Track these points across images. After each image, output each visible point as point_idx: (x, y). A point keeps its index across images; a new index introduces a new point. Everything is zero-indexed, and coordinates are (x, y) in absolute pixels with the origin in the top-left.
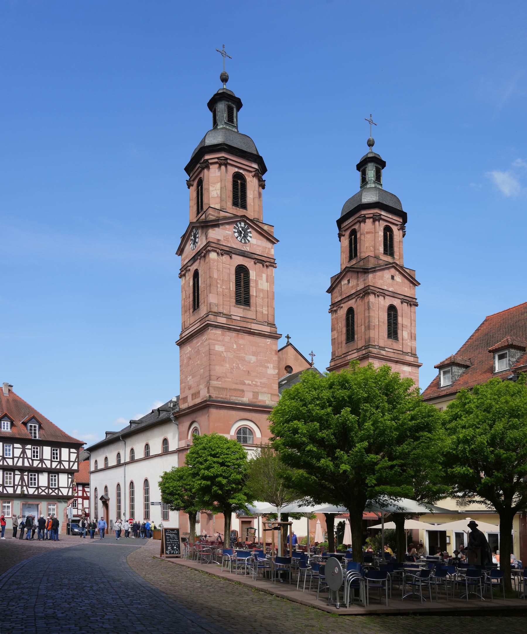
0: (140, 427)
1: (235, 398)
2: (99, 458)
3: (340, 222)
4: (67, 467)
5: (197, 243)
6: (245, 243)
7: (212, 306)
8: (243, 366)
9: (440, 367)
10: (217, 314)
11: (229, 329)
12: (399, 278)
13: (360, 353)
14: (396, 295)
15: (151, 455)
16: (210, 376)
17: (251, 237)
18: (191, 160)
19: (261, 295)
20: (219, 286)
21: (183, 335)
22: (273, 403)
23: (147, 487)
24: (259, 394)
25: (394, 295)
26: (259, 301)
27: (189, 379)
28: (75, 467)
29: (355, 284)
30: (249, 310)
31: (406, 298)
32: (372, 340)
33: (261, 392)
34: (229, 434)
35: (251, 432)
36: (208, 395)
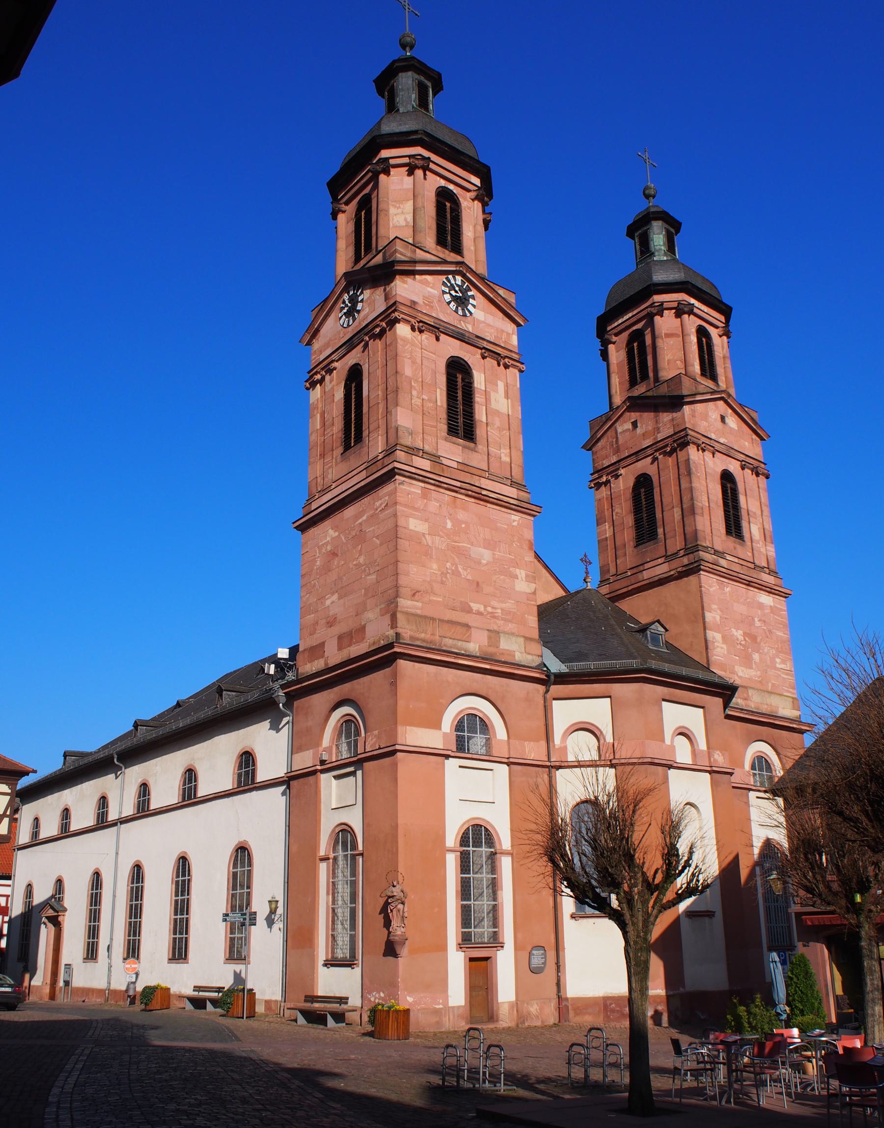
0: (86, 762)
1: (451, 641)
5: (358, 312)
6: (464, 315)
7: (400, 433)
8: (466, 570)
10: (412, 451)
11: (439, 485)
12: (732, 422)
13: (676, 564)
14: (732, 453)
15: (109, 819)
16: (397, 587)
17: (474, 306)
18: (341, 169)
19: (497, 423)
20: (414, 393)
21: (314, 506)
22: (530, 657)
24: (502, 635)
25: (728, 452)
26: (493, 433)
27: (328, 602)
29: (650, 428)
30: (474, 450)
31: (749, 460)
32: (700, 535)
33: (505, 633)
34: (440, 728)
35: (485, 726)
36: (391, 633)
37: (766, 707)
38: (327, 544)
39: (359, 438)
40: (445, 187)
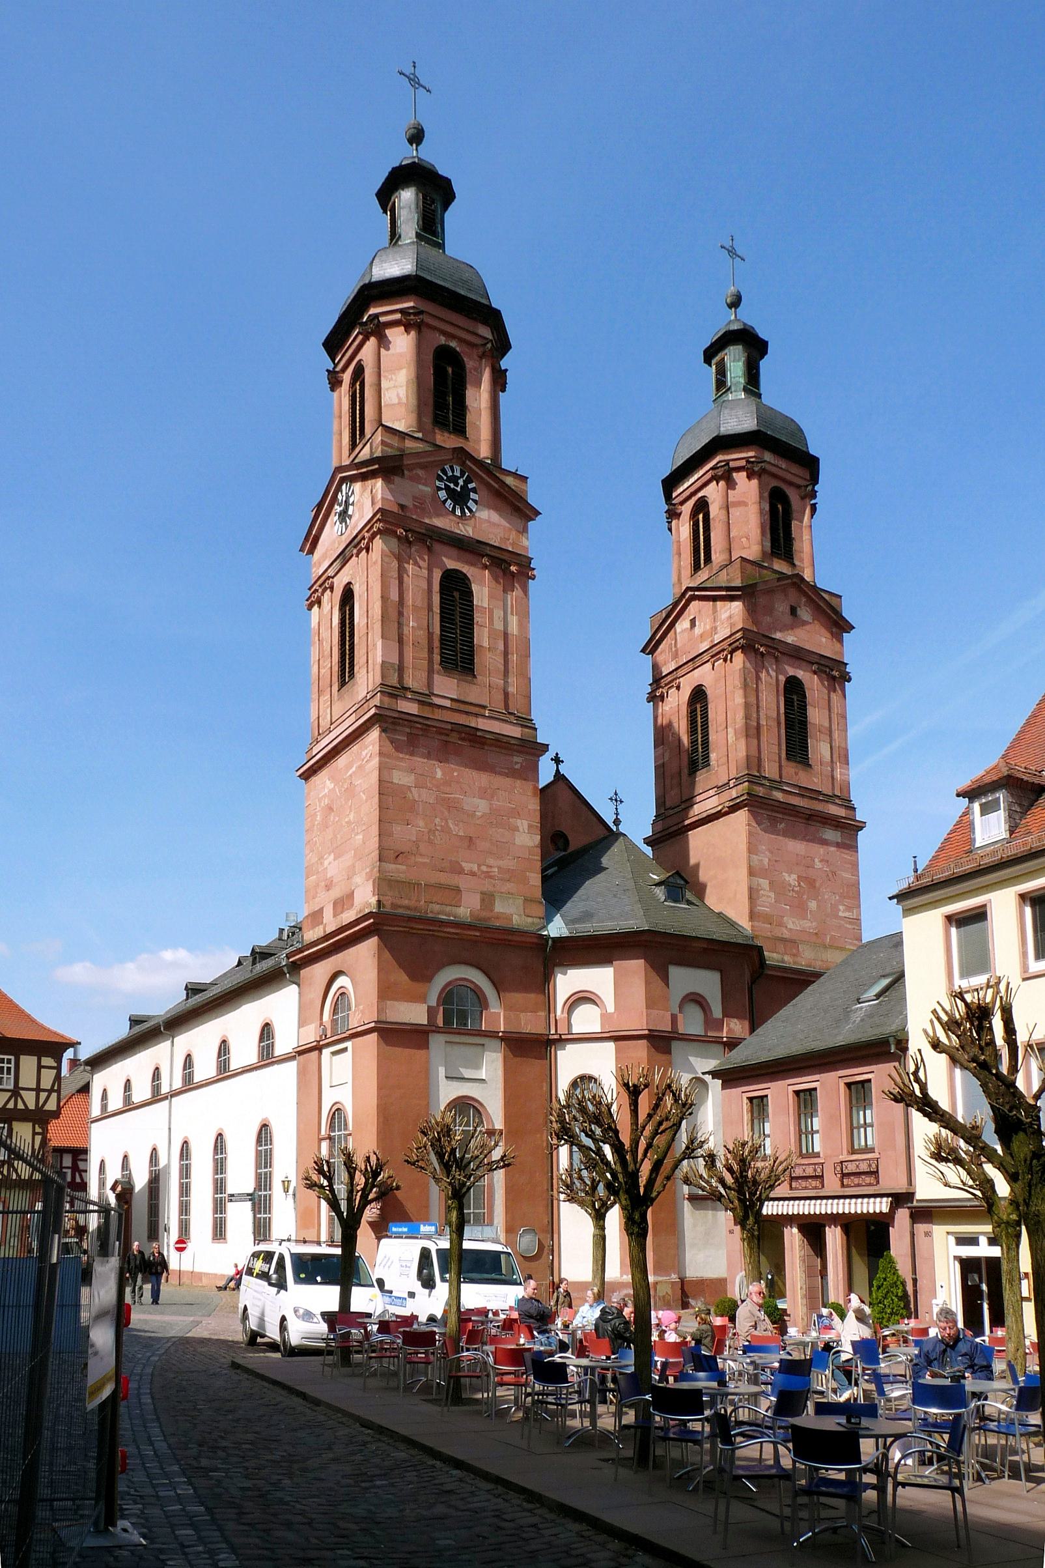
2: (108, 1080)
3: (670, 483)
4: (32, 1106)
5: (350, 517)
9: (971, 794)
17: (475, 502)
22: (530, 920)
23: (222, 1153)
27: (326, 863)
28: (51, 1106)
29: (708, 627)
37: (820, 963)
38: (325, 796)
39: (352, 675)
40: (445, 345)
